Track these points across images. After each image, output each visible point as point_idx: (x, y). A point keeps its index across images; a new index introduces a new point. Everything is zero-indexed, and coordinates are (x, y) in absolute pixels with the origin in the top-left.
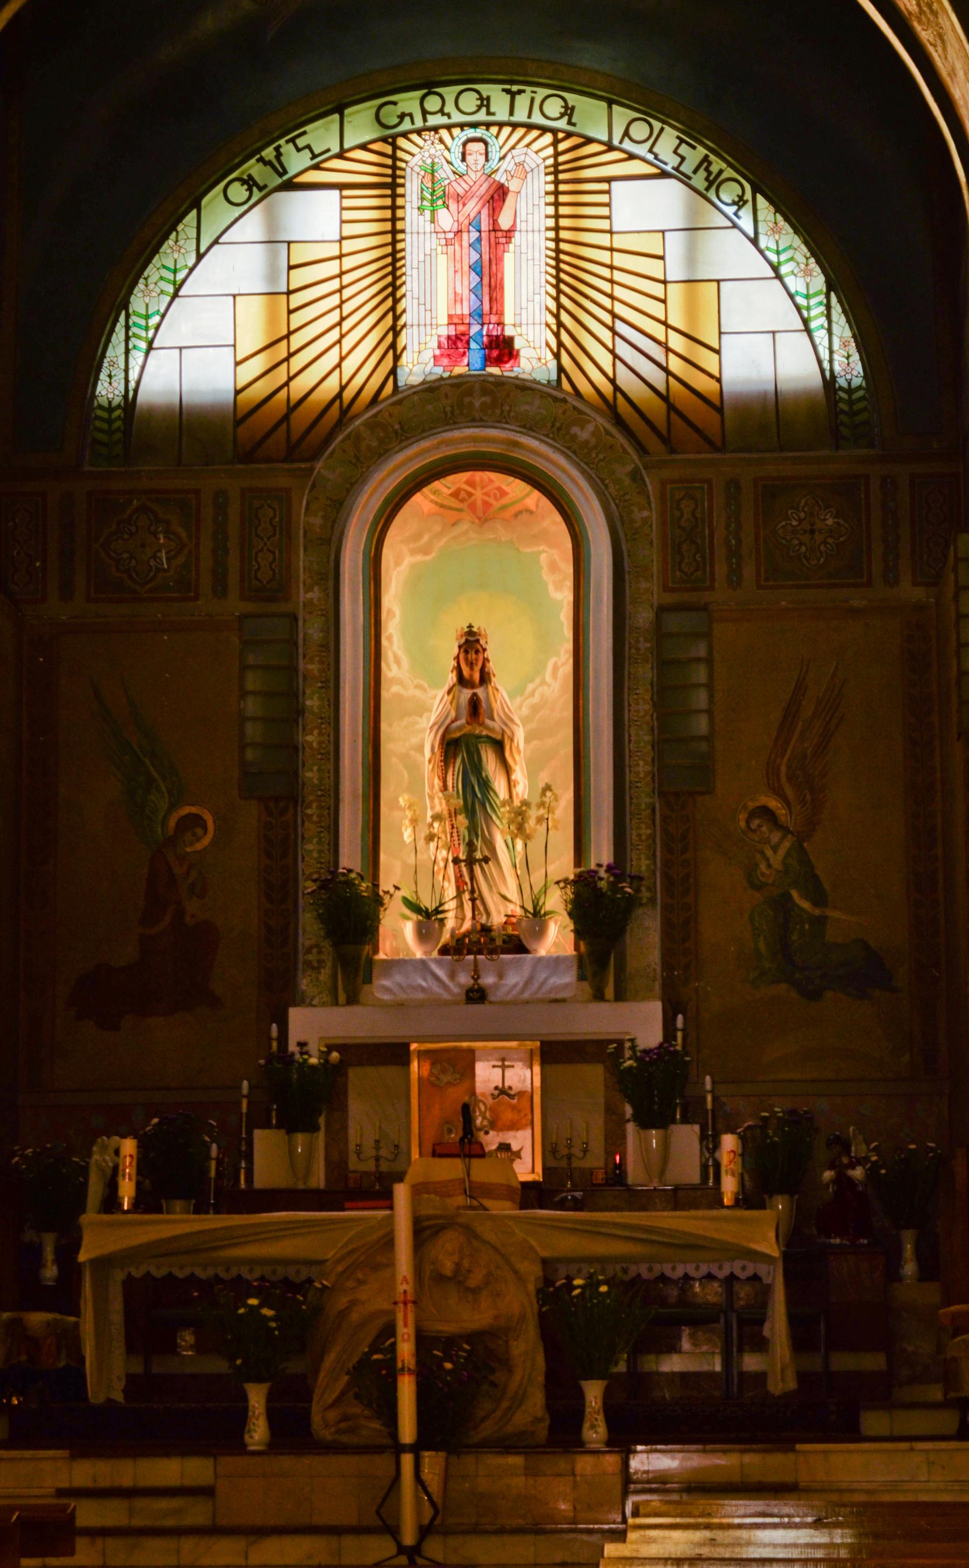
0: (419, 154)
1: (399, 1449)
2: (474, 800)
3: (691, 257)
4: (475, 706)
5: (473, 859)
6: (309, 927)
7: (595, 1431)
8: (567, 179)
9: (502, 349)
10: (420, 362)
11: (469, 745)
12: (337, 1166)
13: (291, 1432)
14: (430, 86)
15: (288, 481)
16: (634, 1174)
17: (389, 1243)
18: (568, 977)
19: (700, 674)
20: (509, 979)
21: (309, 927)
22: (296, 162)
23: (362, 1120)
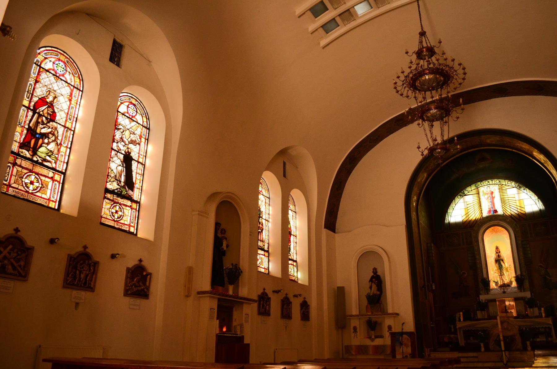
0: (481, 189)
1: (502, 351)
2: (500, 267)
3: (519, 197)
4: (499, 256)
5: (501, 275)
6: (481, 285)
7: (529, 348)
8: (501, 190)
9: (496, 211)
10: (485, 214)
11: (499, 261)
12: (489, 315)
13: (487, 349)
14: (481, 181)
15: (472, 230)
16: (529, 315)
17: (497, 324)
18: (516, 289)
19: (529, 249)
20: (509, 290)
21: (481, 285)
22: (466, 192)
23: (491, 309)
